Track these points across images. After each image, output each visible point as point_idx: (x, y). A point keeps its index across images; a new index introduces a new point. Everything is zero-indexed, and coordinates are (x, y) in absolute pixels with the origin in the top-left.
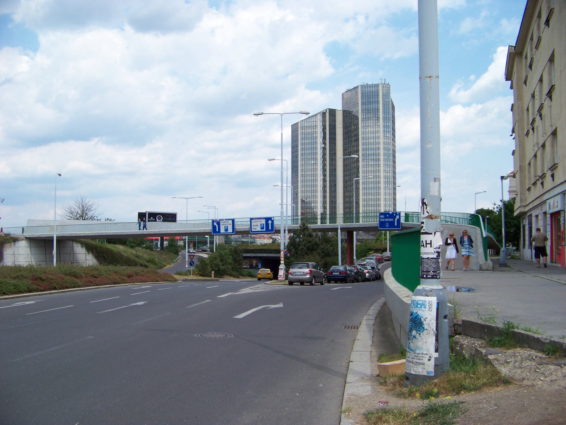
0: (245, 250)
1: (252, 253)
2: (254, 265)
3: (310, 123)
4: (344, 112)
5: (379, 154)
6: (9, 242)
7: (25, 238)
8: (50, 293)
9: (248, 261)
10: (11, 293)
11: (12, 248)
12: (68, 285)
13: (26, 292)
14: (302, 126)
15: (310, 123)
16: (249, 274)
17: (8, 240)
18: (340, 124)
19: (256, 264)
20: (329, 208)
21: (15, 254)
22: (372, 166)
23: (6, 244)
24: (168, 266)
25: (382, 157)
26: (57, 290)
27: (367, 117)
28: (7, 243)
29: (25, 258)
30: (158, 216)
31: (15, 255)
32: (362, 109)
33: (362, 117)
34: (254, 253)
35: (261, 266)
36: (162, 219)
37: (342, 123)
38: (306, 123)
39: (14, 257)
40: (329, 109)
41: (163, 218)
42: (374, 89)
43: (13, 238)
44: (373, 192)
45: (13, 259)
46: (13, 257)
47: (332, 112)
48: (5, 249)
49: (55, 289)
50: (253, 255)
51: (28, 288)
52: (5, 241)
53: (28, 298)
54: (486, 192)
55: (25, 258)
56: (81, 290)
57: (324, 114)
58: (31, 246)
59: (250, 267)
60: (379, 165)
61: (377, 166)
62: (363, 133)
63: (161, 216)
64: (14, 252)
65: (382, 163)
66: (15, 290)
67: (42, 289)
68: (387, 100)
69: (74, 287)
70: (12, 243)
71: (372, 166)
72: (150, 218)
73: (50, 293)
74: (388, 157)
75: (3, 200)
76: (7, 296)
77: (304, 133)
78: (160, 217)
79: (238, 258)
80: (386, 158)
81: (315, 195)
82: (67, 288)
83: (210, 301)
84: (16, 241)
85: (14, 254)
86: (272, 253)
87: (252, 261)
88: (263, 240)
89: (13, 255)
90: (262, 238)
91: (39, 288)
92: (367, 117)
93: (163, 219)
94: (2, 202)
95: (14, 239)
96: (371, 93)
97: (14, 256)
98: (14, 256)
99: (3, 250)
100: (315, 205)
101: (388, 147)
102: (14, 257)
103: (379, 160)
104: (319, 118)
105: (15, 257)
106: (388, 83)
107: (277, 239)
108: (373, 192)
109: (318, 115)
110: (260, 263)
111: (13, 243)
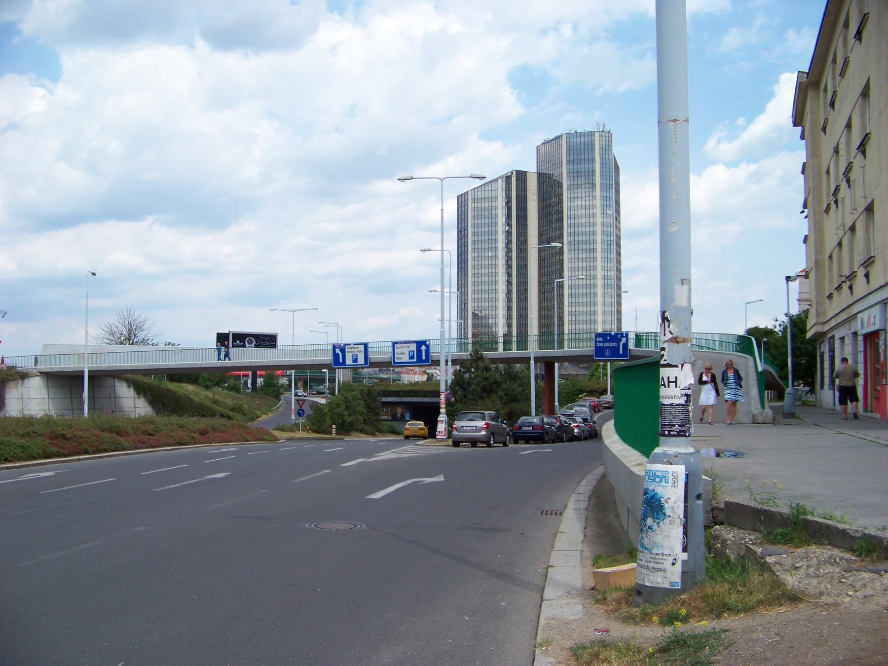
0: (385, 391)
1: (395, 396)
2: (399, 415)
3: (486, 192)
4: (540, 175)
5: (594, 242)
6: (14, 380)
7: (39, 373)
8: (79, 460)
9: (389, 409)
10: (17, 459)
11: (20, 388)
12: (107, 447)
13: (41, 458)
14: (473, 197)
15: (486, 192)
16: (391, 430)
17: (12, 376)
18: (534, 194)
19: (402, 413)
20: (517, 327)
21: (24, 398)
22: (584, 261)
23: (10, 382)
24: (264, 416)
25: (599, 247)
26: (89, 455)
27: (576, 183)
28: (11, 381)
29: (40, 404)
30: (248, 338)
31: (24, 400)
32: (569, 171)
33: (569, 184)
34: (399, 396)
35: (409, 417)
36: (255, 342)
37: (536, 192)
38: (480, 193)
39: (23, 403)
40: (516, 170)
41: (256, 342)
42: (586, 140)
43: (20, 373)
44: (585, 300)
45: (21, 405)
46: (21, 403)
47: (522, 176)
48: (7, 390)
49: (86, 452)
50: (397, 399)
51: (44, 452)
52: (7, 378)
53: (45, 466)
54: (762, 300)
55: (40, 404)
56: (127, 454)
57: (508, 178)
58: (49, 386)
59: (392, 418)
60: (595, 259)
61: (592, 260)
62: (569, 208)
63: (253, 339)
64: (22, 395)
65: (599, 255)
66: (24, 454)
67: (66, 452)
68: (607, 156)
69: (116, 450)
70: (19, 380)
71: (584, 261)
72: (236, 342)
73: (79, 460)
74: (609, 246)
75: (5, 313)
76: (11, 463)
77: (476, 209)
78: (252, 340)
79: (373, 405)
80: (606, 247)
81: (494, 305)
82: (106, 451)
83: (330, 472)
84: (25, 377)
85: (22, 398)
86: (426, 396)
87: (396, 409)
88: (413, 376)
89: (21, 400)
90: (411, 374)
91: (62, 451)
92: (576, 183)
93: (256, 343)
94: (3, 317)
95: (23, 375)
96: (583, 146)
97: (23, 401)
98: (23, 401)
99: (4, 392)
100: (494, 322)
101: (609, 230)
102: (23, 403)
103: (594, 250)
104: (501, 184)
105: (24, 403)
106: (608, 131)
107: (435, 375)
108: (585, 300)
109: (500, 180)
110: (407, 412)
111: (20, 381)
